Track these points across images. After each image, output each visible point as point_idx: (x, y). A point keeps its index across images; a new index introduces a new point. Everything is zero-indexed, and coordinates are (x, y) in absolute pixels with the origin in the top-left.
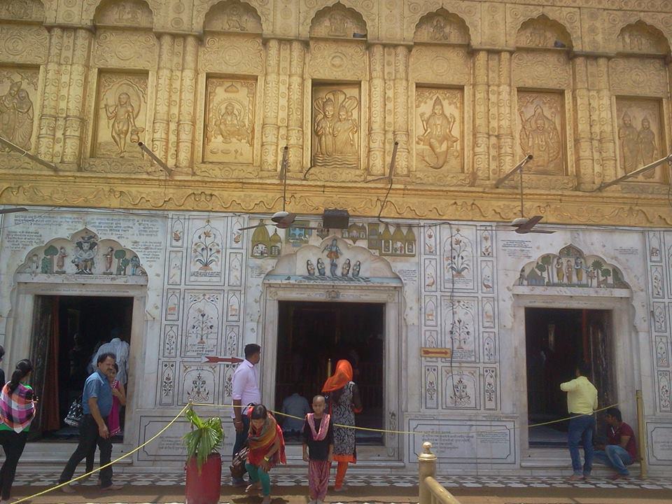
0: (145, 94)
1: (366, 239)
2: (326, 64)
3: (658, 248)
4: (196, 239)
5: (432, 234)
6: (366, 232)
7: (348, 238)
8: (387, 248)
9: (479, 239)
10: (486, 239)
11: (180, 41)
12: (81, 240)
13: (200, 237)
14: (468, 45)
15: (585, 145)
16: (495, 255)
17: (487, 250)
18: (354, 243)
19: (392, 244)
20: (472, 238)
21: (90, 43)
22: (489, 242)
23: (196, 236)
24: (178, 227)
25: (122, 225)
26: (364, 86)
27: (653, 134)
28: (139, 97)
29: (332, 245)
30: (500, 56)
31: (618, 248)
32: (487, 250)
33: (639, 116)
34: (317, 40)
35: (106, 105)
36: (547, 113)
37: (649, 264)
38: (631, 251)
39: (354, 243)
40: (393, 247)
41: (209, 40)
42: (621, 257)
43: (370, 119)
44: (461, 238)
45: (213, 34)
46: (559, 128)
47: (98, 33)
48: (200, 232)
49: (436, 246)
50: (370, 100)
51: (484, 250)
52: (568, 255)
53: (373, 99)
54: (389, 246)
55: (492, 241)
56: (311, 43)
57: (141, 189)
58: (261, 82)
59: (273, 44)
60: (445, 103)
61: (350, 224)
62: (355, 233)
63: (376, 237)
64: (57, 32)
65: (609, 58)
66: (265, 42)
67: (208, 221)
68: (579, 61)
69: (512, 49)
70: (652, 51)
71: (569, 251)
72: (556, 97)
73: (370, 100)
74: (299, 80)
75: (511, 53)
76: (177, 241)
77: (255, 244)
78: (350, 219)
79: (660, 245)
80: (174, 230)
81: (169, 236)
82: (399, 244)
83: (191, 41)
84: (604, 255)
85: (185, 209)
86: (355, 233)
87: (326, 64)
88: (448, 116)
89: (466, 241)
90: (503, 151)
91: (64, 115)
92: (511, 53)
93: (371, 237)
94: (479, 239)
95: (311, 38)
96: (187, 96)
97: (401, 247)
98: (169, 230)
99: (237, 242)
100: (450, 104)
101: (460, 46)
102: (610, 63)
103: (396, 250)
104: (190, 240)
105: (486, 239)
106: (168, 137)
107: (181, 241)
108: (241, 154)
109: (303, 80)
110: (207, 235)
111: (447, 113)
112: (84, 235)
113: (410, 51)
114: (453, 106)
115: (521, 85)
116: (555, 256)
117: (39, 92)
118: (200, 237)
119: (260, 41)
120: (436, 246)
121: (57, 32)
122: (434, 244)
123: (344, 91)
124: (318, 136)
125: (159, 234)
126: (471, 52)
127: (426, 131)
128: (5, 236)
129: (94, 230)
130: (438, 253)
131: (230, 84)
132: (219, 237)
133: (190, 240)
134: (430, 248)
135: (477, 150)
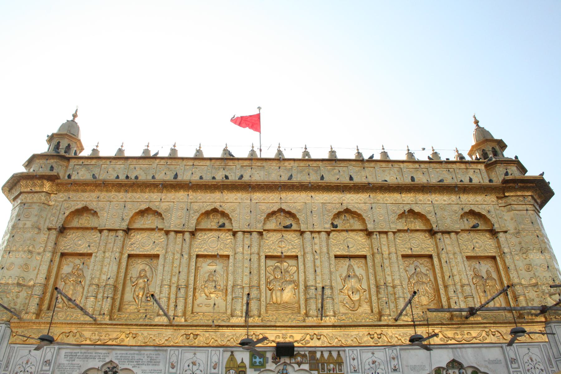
0: (156, 269)
1: (307, 363)
2: (274, 244)
3: (515, 358)
4: (186, 367)
5: (355, 357)
6: (307, 359)
7: (295, 363)
8: (323, 369)
9: (388, 359)
10: (394, 358)
11: (247, 235)
12: (108, 370)
13: (189, 366)
14: (366, 230)
15: (451, 289)
16: (401, 370)
17: (395, 367)
18: (299, 366)
19: (327, 366)
20: (383, 358)
21: (124, 239)
22: (396, 360)
23: (186, 365)
24: (174, 359)
25: (136, 358)
26: (300, 259)
27: (495, 280)
28: (152, 272)
29: (283, 369)
30: (387, 235)
31: (487, 360)
32: (395, 367)
33: (485, 267)
34: (268, 231)
35: (131, 278)
36: (424, 270)
37: (511, 370)
38: (496, 362)
39: (299, 366)
40: (327, 369)
41: (199, 235)
42: (490, 366)
43: (305, 279)
44: (375, 359)
45: (202, 230)
46: (432, 279)
47: (130, 233)
48: (190, 362)
49: (358, 365)
50: (305, 266)
51: (393, 367)
52: (453, 367)
53: (307, 266)
54: (324, 368)
55: (398, 360)
56: (264, 233)
57: (150, 333)
58: (231, 259)
59: (240, 235)
60: (355, 267)
61: (295, 353)
62: (299, 359)
63: (315, 362)
64: (105, 232)
65: (457, 233)
66: (235, 234)
67: (195, 354)
68: (439, 236)
69: (394, 231)
70: (424, 228)
71: (454, 364)
72: (427, 260)
73: (305, 266)
74: (257, 257)
75: (394, 233)
76: (173, 368)
77: (228, 369)
78: (295, 349)
79: (516, 356)
80: (171, 361)
81: (167, 365)
82: (332, 366)
83: (255, 235)
84: (478, 365)
85: (258, 196)
86: (299, 359)
87: (274, 244)
88: (358, 275)
89: (379, 361)
90: (397, 296)
91: (104, 284)
92: (394, 233)
93: (311, 361)
94: (388, 359)
95: (265, 230)
96: (184, 270)
97: (334, 369)
98: (168, 360)
99: (215, 369)
100: (358, 267)
101: (361, 230)
102: (458, 236)
103: (330, 370)
104: (182, 368)
105: (394, 358)
106: (170, 296)
107: (175, 369)
108: (218, 307)
109: (259, 257)
110: (194, 364)
111: (358, 274)
112: (109, 365)
113: (329, 235)
114: (360, 269)
115: (404, 253)
116: (444, 368)
117: (90, 271)
118: (189, 366)
119: (231, 233)
120: (358, 365)
121: (105, 232)
122: (356, 365)
123: (287, 261)
124: (270, 290)
125: (161, 364)
126: (369, 234)
127: (344, 286)
128: (56, 367)
129: (116, 362)
130: (360, 371)
131: (211, 261)
132: (202, 365)
133: (182, 368)
134: (354, 368)
135: (380, 296)
